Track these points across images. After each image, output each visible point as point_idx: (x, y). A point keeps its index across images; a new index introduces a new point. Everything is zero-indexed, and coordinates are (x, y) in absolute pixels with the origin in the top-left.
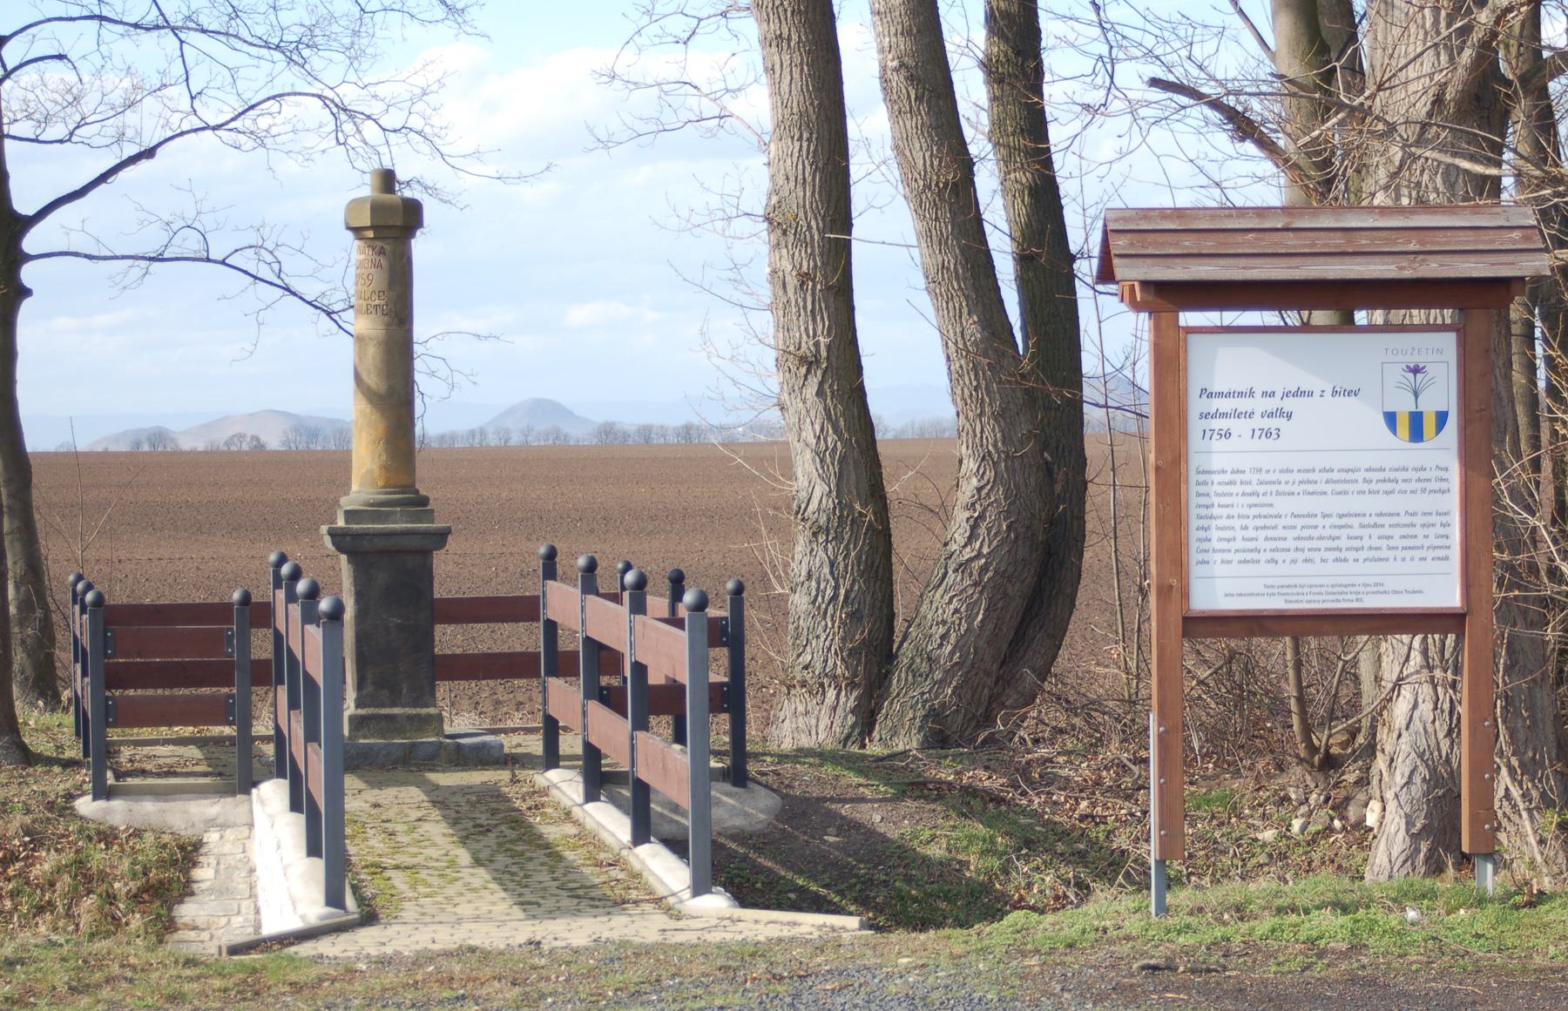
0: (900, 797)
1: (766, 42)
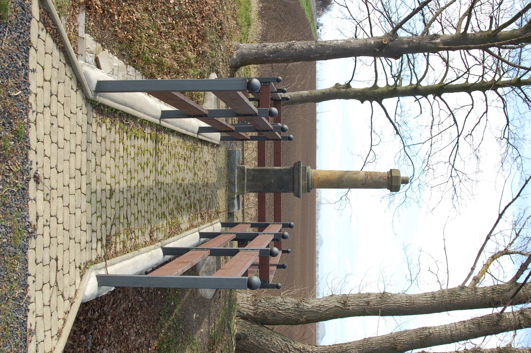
0: (211, 338)
1: (433, 293)
